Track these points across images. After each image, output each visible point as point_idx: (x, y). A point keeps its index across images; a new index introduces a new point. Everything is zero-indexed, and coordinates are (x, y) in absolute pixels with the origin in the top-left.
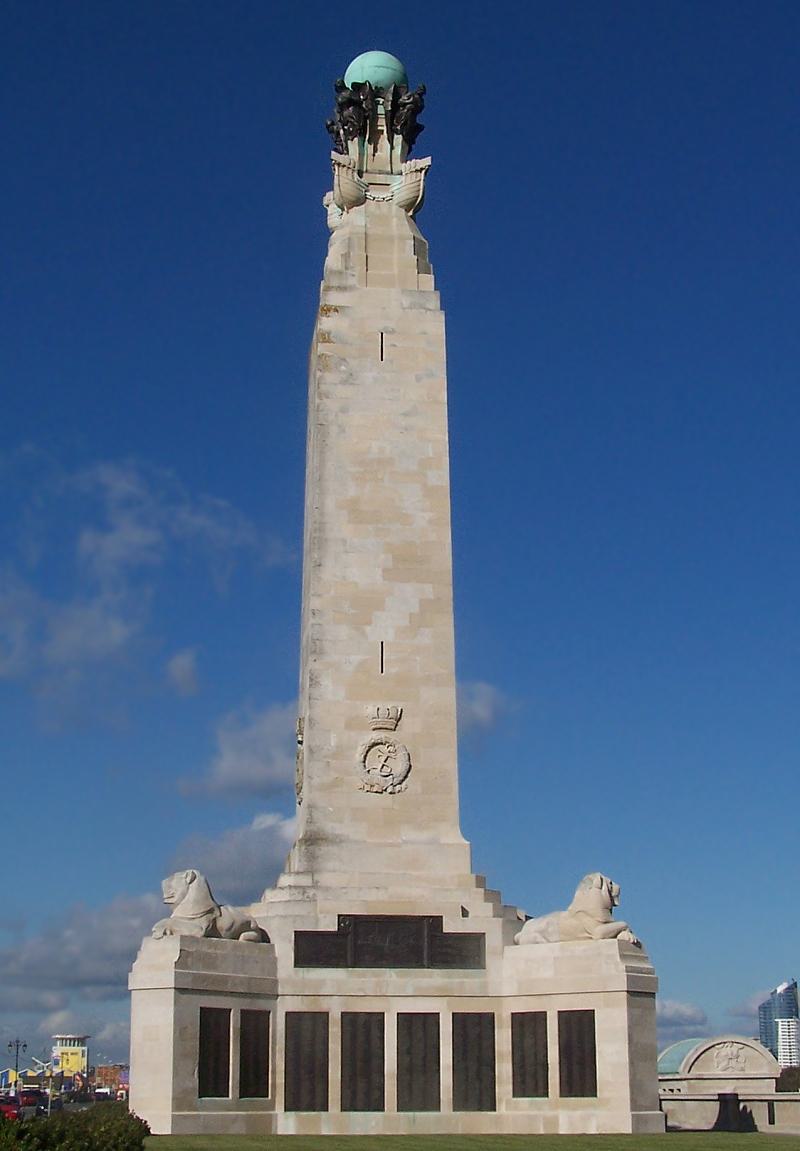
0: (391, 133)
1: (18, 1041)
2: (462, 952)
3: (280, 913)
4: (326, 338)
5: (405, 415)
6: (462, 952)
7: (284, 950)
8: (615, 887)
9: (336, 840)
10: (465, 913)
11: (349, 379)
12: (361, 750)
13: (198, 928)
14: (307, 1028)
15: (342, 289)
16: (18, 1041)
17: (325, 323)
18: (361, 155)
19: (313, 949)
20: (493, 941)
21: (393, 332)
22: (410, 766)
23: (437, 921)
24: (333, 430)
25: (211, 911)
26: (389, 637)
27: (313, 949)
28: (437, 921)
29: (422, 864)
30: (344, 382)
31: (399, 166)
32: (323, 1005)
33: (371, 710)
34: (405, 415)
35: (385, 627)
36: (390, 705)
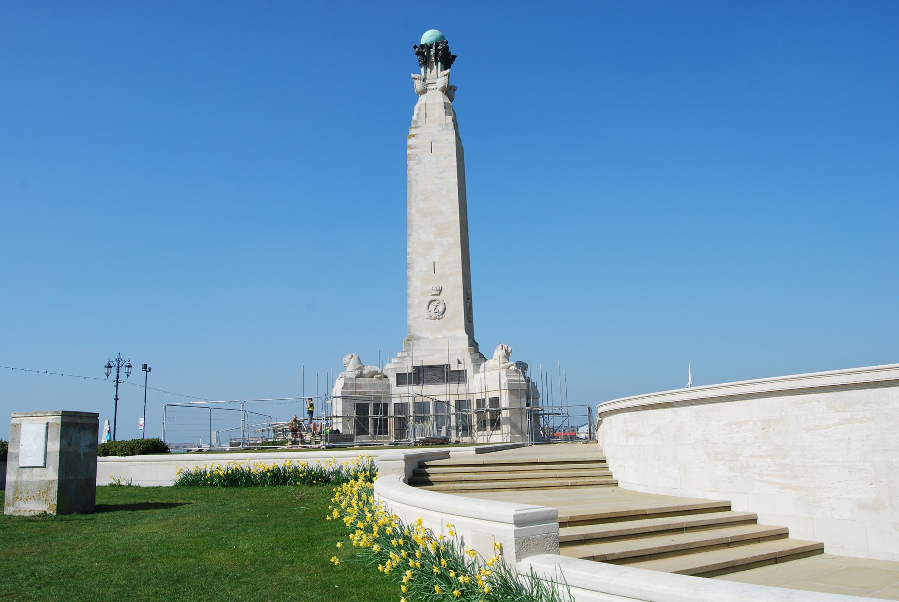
0: (437, 62)
1: (119, 360)
2: (459, 377)
3: (391, 369)
4: (411, 147)
5: (441, 173)
6: (459, 377)
7: (393, 380)
8: (510, 349)
9: (418, 339)
10: (459, 362)
11: (419, 162)
12: (427, 304)
13: (352, 375)
14: (401, 408)
15: (416, 127)
16: (119, 360)
17: (410, 142)
18: (426, 73)
19: (402, 379)
20: (470, 373)
21: (436, 141)
22: (445, 309)
23: (448, 366)
24: (414, 183)
25: (360, 368)
26: (437, 260)
27: (402, 379)
28: (448, 366)
29: (444, 343)
30: (417, 164)
31: (440, 74)
32: (404, 400)
33: (430, 288)
34: (441, 173)
35: (435, 256)
36: (438, 286)
